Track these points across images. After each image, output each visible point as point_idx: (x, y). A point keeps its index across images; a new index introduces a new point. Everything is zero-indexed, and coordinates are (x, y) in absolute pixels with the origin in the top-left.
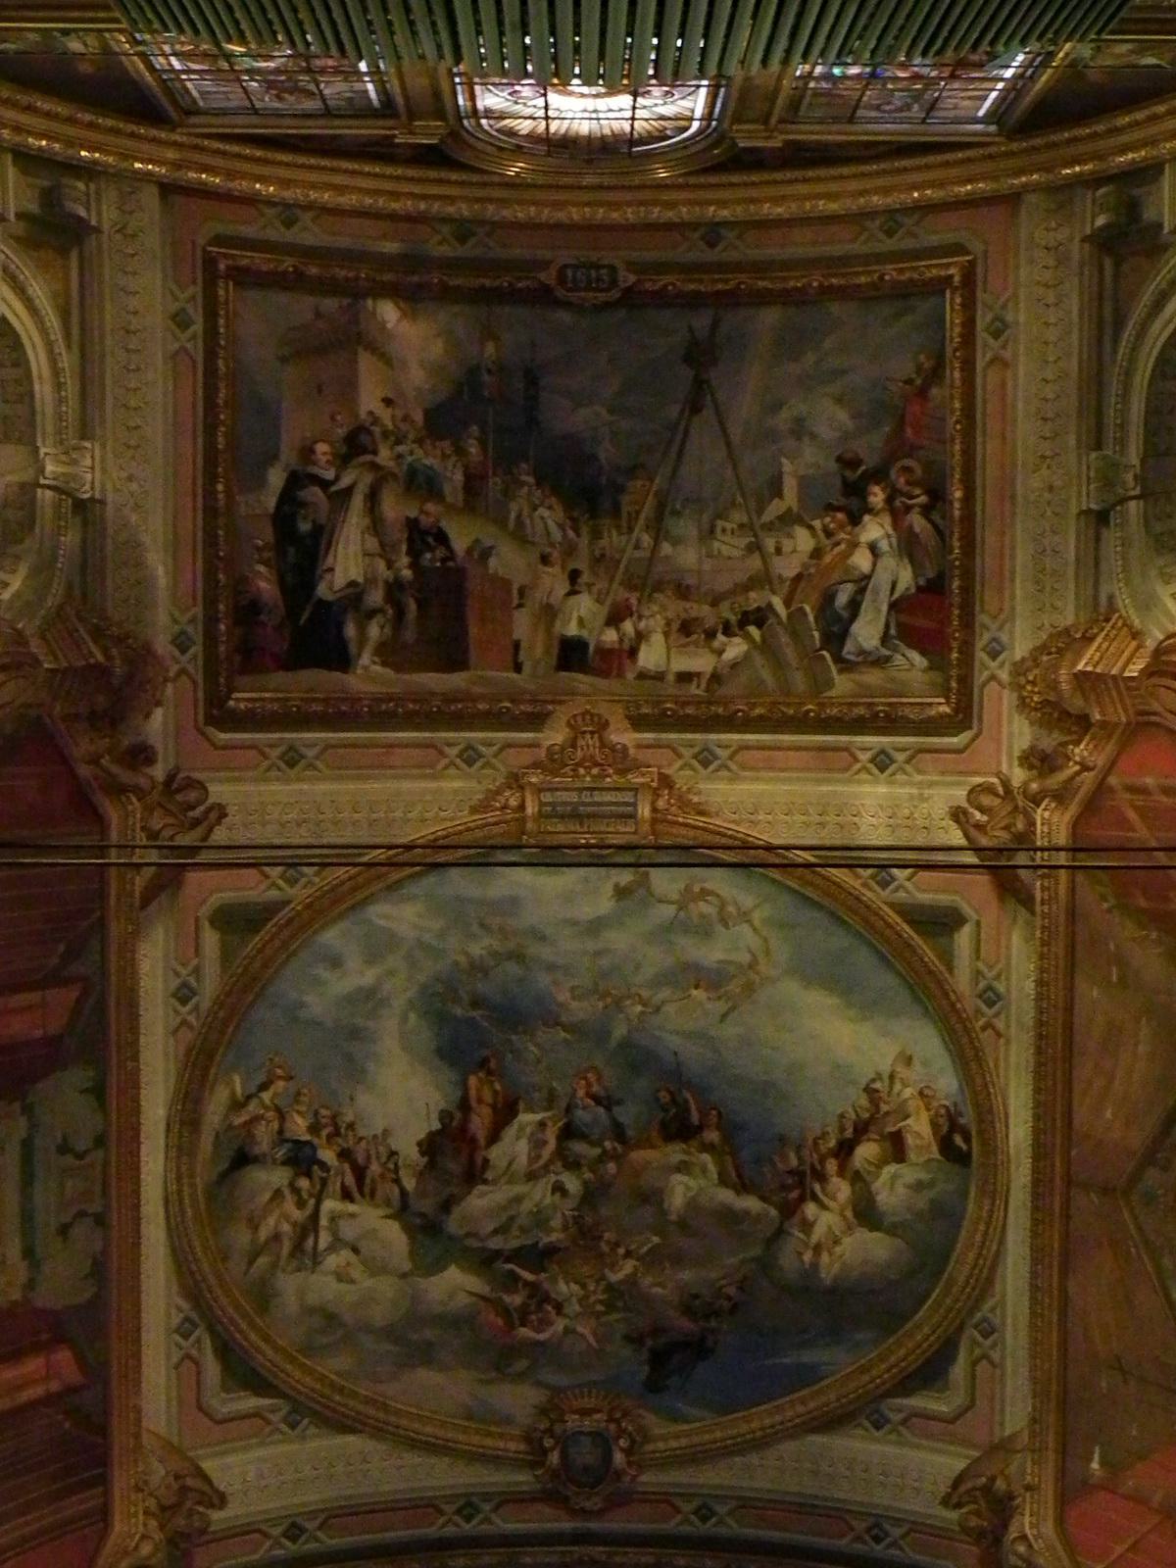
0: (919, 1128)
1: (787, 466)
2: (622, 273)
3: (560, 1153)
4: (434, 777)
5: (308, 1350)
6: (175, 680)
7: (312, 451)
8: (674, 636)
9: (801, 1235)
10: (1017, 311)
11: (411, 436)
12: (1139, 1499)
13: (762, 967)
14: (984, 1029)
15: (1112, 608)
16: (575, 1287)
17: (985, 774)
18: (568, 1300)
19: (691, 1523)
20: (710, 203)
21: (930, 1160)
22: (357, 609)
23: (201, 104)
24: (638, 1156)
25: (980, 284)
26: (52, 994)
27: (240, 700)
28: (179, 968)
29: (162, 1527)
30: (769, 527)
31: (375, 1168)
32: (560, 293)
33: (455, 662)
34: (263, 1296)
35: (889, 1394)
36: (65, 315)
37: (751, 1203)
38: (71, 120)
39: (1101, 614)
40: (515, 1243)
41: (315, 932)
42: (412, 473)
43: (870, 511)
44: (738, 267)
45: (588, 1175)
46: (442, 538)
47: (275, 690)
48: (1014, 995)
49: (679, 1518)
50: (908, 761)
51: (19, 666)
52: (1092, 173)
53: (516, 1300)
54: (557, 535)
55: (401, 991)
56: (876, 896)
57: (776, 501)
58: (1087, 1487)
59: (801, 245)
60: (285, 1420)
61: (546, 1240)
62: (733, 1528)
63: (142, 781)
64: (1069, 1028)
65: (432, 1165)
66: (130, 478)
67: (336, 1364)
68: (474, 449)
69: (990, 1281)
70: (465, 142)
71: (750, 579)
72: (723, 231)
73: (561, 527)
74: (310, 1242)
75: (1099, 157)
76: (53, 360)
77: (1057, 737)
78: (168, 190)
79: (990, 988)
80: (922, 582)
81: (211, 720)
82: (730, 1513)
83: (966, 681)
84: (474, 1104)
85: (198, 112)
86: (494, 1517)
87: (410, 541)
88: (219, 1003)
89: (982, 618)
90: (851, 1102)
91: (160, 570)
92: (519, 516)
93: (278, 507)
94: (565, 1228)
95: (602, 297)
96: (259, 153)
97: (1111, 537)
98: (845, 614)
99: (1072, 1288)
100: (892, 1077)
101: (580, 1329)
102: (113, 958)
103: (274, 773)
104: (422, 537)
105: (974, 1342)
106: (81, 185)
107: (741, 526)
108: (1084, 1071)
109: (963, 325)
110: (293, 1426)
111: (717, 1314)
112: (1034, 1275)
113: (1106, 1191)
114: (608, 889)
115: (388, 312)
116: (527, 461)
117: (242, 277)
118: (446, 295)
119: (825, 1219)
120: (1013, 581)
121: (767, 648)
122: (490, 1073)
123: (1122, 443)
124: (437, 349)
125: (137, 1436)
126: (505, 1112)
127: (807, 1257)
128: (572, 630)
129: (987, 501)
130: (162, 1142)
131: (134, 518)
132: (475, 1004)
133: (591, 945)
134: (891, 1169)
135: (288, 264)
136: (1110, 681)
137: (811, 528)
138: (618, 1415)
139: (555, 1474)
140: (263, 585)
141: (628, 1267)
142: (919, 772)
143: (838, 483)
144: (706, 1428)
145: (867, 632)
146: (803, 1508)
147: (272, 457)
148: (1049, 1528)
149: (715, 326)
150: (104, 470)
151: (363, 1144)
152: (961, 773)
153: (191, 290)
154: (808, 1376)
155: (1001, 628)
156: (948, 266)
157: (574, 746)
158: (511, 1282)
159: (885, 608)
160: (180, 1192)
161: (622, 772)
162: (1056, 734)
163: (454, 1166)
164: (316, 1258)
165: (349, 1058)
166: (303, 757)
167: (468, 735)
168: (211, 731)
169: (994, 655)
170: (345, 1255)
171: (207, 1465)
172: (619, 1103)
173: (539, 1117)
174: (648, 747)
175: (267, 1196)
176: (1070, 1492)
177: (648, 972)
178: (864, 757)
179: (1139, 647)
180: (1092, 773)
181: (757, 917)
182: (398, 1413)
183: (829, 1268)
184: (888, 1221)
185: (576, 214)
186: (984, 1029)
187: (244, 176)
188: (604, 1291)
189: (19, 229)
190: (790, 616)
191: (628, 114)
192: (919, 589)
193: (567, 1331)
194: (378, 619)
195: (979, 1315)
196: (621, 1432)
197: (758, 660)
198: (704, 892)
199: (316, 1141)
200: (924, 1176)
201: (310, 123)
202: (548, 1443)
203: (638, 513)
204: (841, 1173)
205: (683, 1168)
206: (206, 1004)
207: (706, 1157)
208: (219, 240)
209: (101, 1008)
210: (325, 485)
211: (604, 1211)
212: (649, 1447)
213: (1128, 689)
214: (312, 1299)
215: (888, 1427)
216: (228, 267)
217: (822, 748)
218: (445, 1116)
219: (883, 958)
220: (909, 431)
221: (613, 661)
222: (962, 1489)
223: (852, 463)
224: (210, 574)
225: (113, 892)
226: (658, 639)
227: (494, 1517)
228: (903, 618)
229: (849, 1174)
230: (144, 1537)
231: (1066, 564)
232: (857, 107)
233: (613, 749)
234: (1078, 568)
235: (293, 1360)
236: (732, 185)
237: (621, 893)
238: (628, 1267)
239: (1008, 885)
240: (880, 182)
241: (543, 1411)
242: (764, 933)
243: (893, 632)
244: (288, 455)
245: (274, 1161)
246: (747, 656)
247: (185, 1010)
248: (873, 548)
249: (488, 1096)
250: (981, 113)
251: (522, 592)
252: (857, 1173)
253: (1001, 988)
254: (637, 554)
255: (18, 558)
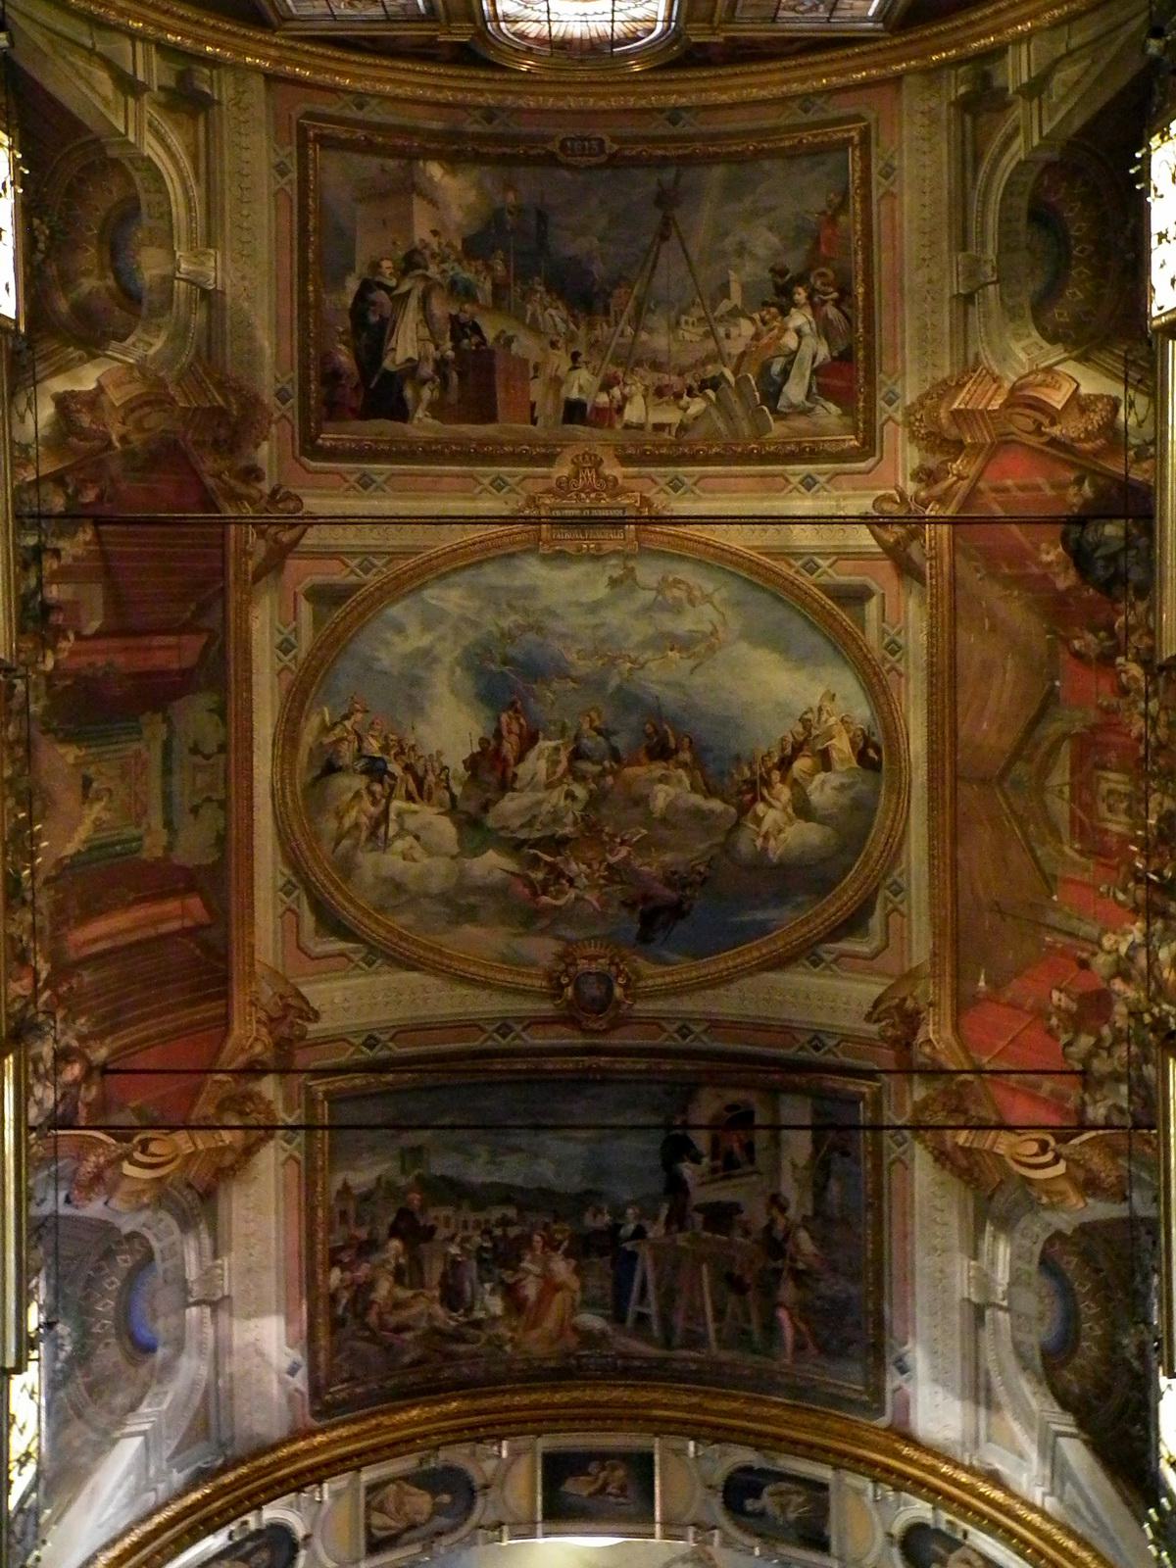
0: (841, 746)
1: (733, 276)
2: (608, 143)
3: (571, 770)
4: (473, 499)
5: (381, 909)
6: (276, 422)
7: (380, 266)
8: (650, 398)
9: (754, 827)
10: (901, 158)
11: (453, 257)
12: (1014, 1005)
13: (721, 635)
14: (889, 672)
15: (977, 361)
16: (583, 867)
17: (885, 488)
18: (579, 875)
19: (675, 1040)
20: (672, 93)
21: (852, 769)
22: (413, 378)
23: (294, 11)
24: (630, 771)
25: (873, 141)
26: (185, 639)
27: (327, 439)
28: (282, 628)
29: (270, 1033)
30: (721, 320)
31: (431, 778)
32: (562, 157)
33: (490, 417)
34: (347, 868)
35: (822, 941)
36: (194, 158)
37: (716, 805)
38: (198, 23)
39: (969, 368)
40: (538, 835)
41: (386, 606)
42: (454, 283)
43: (795, 305)
44: (691, 138)
45: (593, 786)
46: (477, 330)
47: (352, 434)
48: (911, 646)
49: (665, 1035)
50: (828, 481)
51: (161, 402)
52: (955, 57)
53: (539, 876)
54: (562, 327)
55: (449, 653)
56: (806, 581)
57: (725, 301)
58: (976, 1000)
59: (738, 122)
60: (363, 959)
61: (561, 832)
62: (708, 1043)
63: (254, 493)
64: (953, 666)
65: (474, 777)
66: (243, 278)
67: (402, 920)
68: (500, 267)
69: (897, 855)
70: (488, 41)
71: (707, 357)
72: (684, 114)
73: (565, 321)
74: (382, 829)
75: (959, 44)
76: (186, 190)
77: (939, 458)
78: (271, 79)
79: (893, 642)
80: (835, 354)
81: (304, 452)
82: (705, 1031)
83: (870, 423)
84: (505, 733)
85: (293, 19)
86: (524, 1035)
87: (452, 331)
88: (311, 655)
89: (880, 377)
90: (788, 729)
91: (265, 342)
92: (533, 315)
93: (355, 303)
94: (575, 823)
95: (593, 160)
96: (337, 54)
97: (975, 313)
98: (779, 380)
99: (960, 856)
100: (820, 709)
101: (587, 897)
102: (232, 616)
103: (352, 493)
104: (460, 328)
105: (886, 899)
106: (206, 71)
107: (700, 319)
108: (963, 698)
109: (862, 171)
110: (370, 965)
111: (691, 885)
112: (931, 847)
113: (983, 781)
114: (605, 580)
115: (435, 170)
116: (539, 275)
117: (326, 142)
118: (479, 159)
119: (771, 816)
120: (903, 348)
121: (720, 404)
122: (516, 711)
123: (983, 245)
124: (472, 196)
125: (252, 965)
126: (529, 740)
127: (759, 842)
128: (575, 395)
129: (883, 296)
130: (270, 754)
131: (246, 305)
132: (506, 661)
133: (593, 620)
134: (821, 776)
135: (360, 134)
136: (978, 416)
137: (752, 320)
138: (617, 960)
139: (570, 1004)
140: (343, 358)
141: (624, 852)
142: (837, 489)
143: (770, 285)
144: (686, 970)
145: (795, 391)
146: (760, 1027)
147: (350, 268)
148: (947, 1033)
149: (678, 176)
150: (223, 270)
151: (422, 761)
152: (867, 488)
153: (289, 149)
154: (762, 929)
155: (895, 383)
156: (849, 130)
157: (577, 477)
158: (535, 862)
159: (808, 373)
160: (283, 789)
161: (614, 496)
162: (938, 456)
163: (492, 778)
164: (387, 842)
165: (410, 698)
166: (374, 481)
167: (496, 469)
168: (305, 460)
169: (890, 403)
170: (410, 839)
171: (304, 990)
172: (615, 733)
173: (552, 744)
174: (634, 477)
175: (350, 795)
176: (962, 1005)
177: (636, 638)
178: (795, 480)
179: (999, 387)
180: (966, 482)
181: (717, 598)
182: (451, 957)
183: (776, 850)
184: (820, 812)
185: (572, 103)
186: (889, 672)
187: (327, 70)
188: (606, 869)
189: (162, 97)
190: (737, 382)
191: (609, 17)
192: (834, 359)
193: (578, 899)
194: (429, 385)
195: (889, 881)
196: (620, 973)
197: (715, 413)
198: (677, 582)
199: (386, 757)
200: (845, 780)
201: (377, 26)
202: (564, 980)
203: (622, 312)
204: (783, 781)
205: (664, 780)
206: (303, 655)
207: (681, 772)
208: (309, 115)
209: (223, 651)
210: (388, 290)
211: (605, 811)
212: (642, 984)
213: (991, 418)
214: (384, 873)
215: (822, 965)
216: (316, 135)
217: (763, 476)
218: (483, 741)
219: (811, 625)
220: (823, 249)
221: (604, 417)
222: (883, 1007)
223: (782, 273)
224: (303, 349)
225: (232, 572)
226: (638, 400)
227: (524, 1035)
228: (821, 380)
229: (789, 780)
230: (256, 1039)
231: (943, 334)
232: (778, 9)
233: (606, 479)
234: (951, 336)
235: (369, 915)
236: (688, 80)
237: (614, 583)
238: (624, 852)
239: (906, 569)
240: (799, 73)
241: (561, 957)
242: (722, 609)
243: (814, 390)
244: (361, 268)
245: (355, 770)
246: (706, 412)
247: (286, 658)
248: (799, 332)
249: (515, 728)
250: (871, 13)
251: (536, 368)
252: (795, 781)
253: (901, 641)
254: (622, 340)
255: (159, 328)
